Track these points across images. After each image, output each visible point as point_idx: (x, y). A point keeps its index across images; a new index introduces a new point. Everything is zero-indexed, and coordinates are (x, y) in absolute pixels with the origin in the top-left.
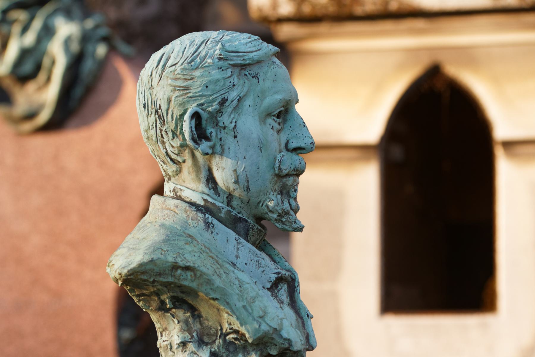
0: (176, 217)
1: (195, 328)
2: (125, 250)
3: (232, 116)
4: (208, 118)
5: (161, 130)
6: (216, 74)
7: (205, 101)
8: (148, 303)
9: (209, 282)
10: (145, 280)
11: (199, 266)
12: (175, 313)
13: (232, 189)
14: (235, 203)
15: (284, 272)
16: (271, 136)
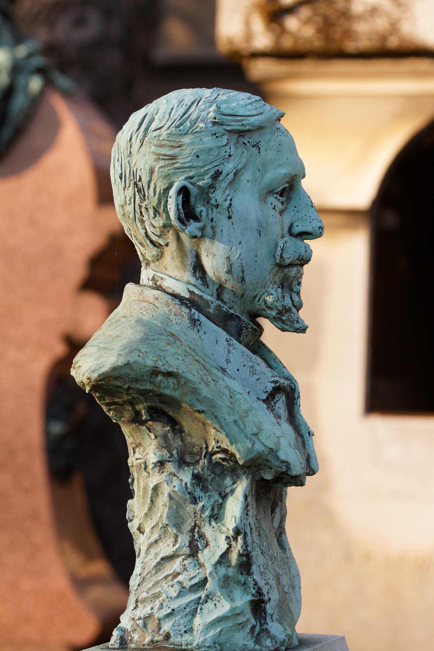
0: (155, 311)
1: (176, 445)
2: (95, 349)
3: (227, 192)
4: (198, 193)
5: (140, 207)
6: (209, 142)
7: (195, 173)
8: (120, 413)
9: (195, 391)
10: (118, 387)
11: (183, 372)
12: (152, 426)
13: (223, 279)
14: (226, 296)
15: (282, 381)
16: (273, 217)
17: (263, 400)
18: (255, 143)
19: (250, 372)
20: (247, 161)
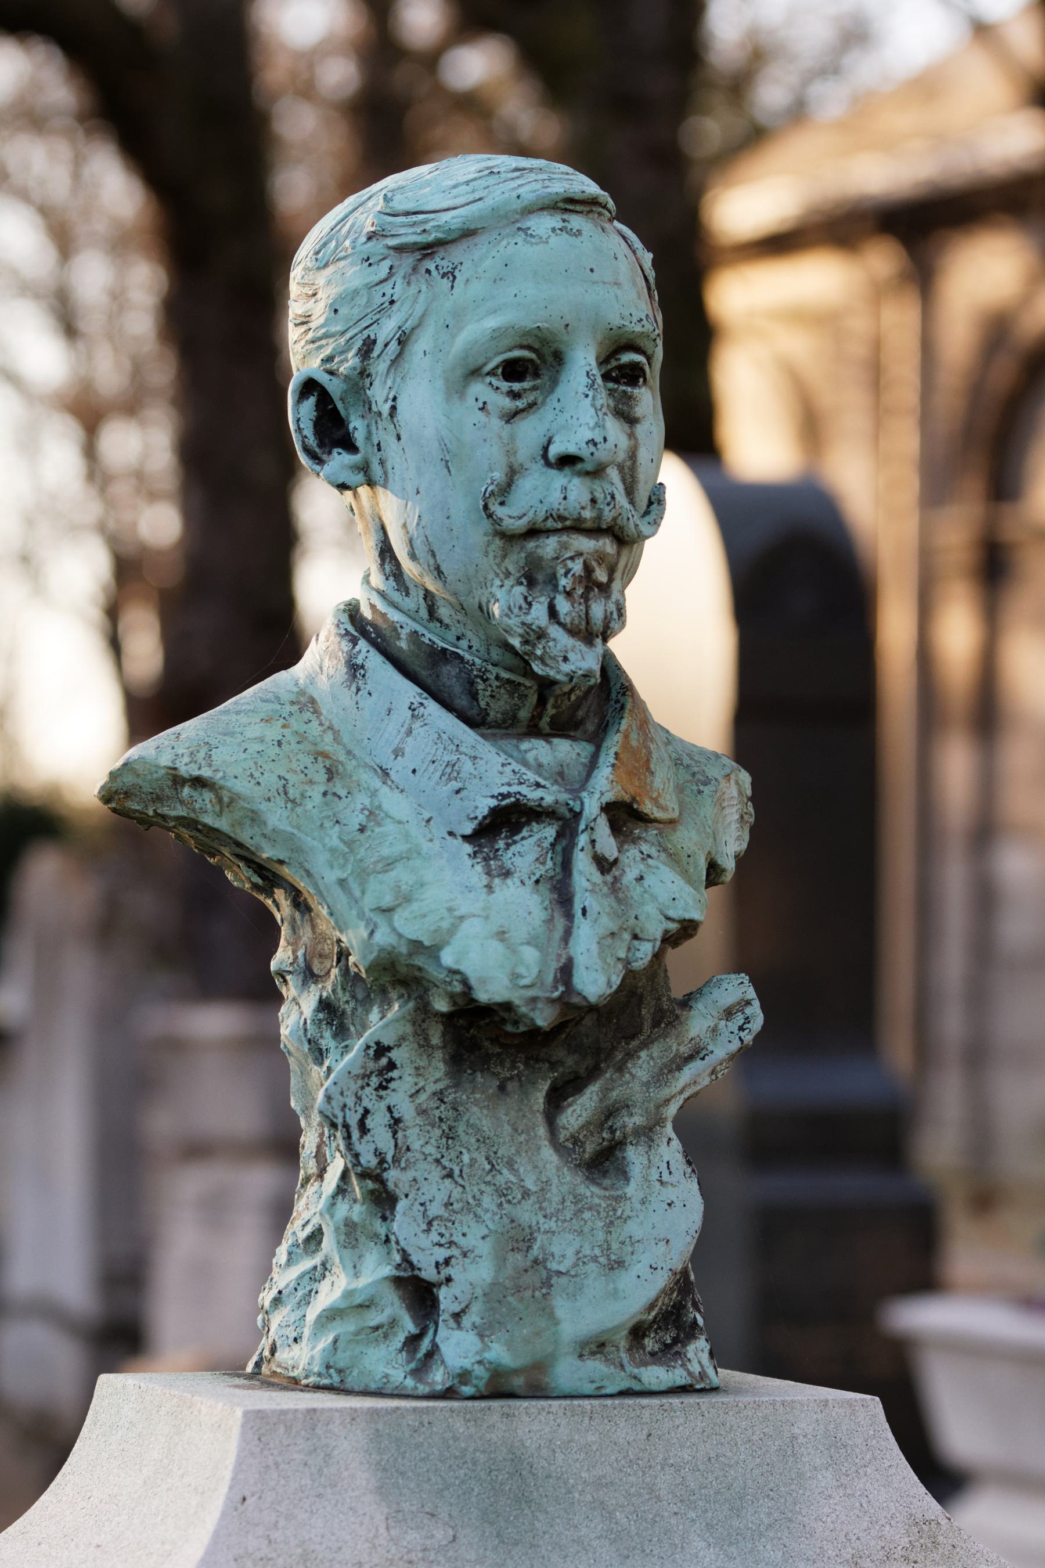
3: (389, 383)
4: (345, 392)
7: (334, 349)
17: (465, 838)
18: (449, 269)
19: (443, 774)
20: (426, 310)
